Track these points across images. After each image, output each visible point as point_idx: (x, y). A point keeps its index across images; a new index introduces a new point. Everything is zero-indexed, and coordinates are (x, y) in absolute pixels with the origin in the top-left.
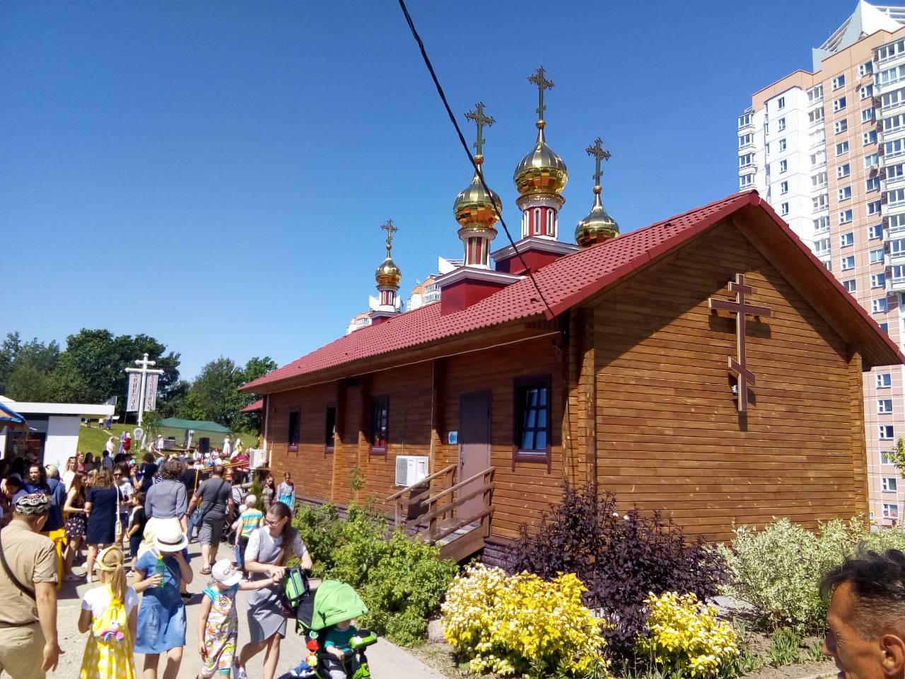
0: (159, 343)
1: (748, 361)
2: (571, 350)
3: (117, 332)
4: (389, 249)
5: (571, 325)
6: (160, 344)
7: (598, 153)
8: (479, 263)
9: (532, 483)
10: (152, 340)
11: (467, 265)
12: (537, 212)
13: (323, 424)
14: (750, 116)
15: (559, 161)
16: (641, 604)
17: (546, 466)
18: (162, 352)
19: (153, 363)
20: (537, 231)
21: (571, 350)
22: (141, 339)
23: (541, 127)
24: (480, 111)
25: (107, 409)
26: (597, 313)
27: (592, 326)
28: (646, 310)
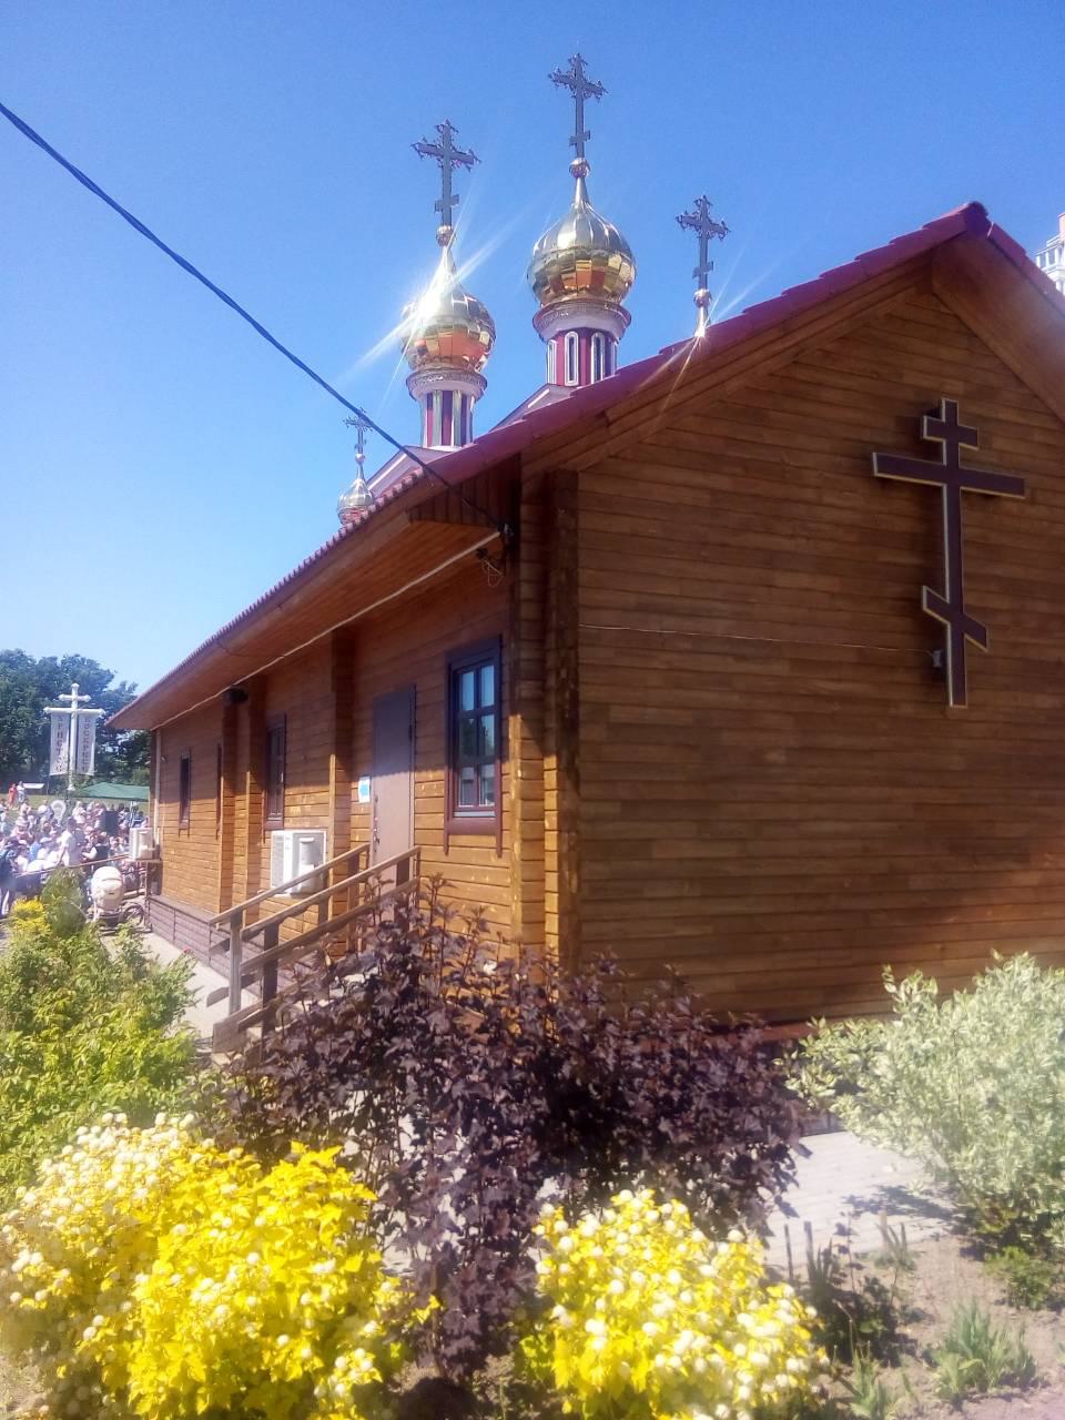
0: (103, 667)
1: (968, 599)
2: (525, 571)
3: (37, 653)
4: (360, 462)
5: (524, 511)
6: (105, 669)
7: (703, 224)
8: (449, 444)
9: (473, 879)
10: (92, 664)
11: (425, 446)
12: (572, 340)
13: (215, 774)
14: (1056, 252)
15: (611, 231)
16: (266, 1375)
17: (492, 841)
18: (109, 681)
19: (86, 698)
20: (571, 379)
21: (525, 571)
22: (74, 662)
23: (578, 173)
24: (447, 138)
25: (91, 772)
26: (584, 484)
27: (573, 513)
28: (722, 482)
